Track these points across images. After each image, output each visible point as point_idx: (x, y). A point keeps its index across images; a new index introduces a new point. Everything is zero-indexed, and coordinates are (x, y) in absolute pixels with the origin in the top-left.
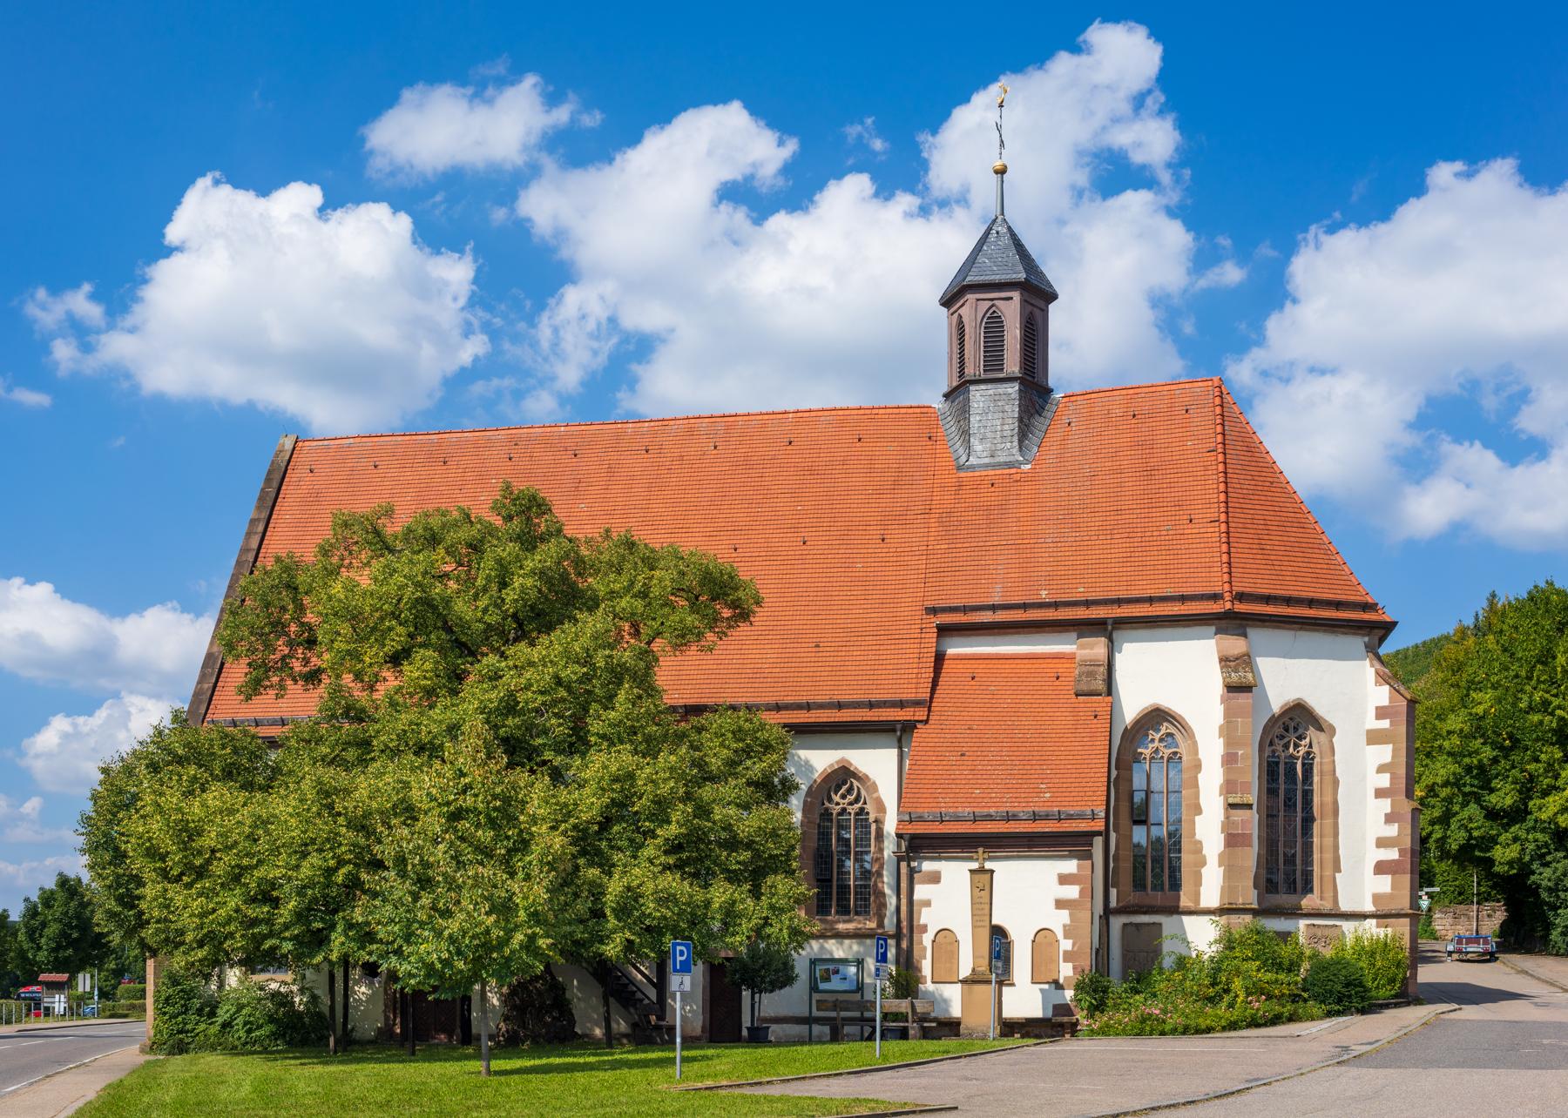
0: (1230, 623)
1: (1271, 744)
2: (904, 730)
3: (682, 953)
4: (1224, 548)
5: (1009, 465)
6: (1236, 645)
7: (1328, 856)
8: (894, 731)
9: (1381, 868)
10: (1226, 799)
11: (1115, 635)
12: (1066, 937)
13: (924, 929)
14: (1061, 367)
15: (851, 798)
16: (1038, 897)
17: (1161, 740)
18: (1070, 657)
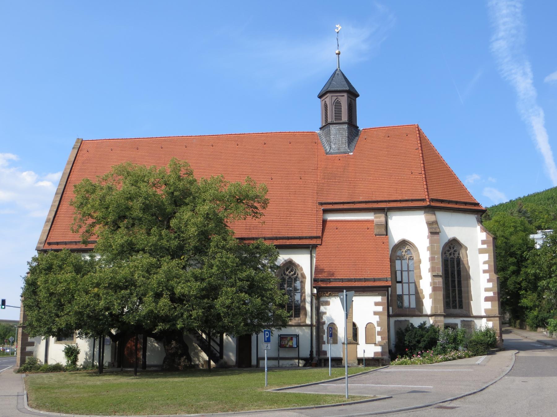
0: (430, 209)
1: (445, 253)
2: (312, 248)
3: (267, 335)
4: (425, 183)
5: (345, 153)
6: (432, 218)
9: (487, 299)
11: (388, 213)
12: (378, 326)
14: (362, 123)
16: (368, 310)
17: (406, 252)
18: (372, 221)
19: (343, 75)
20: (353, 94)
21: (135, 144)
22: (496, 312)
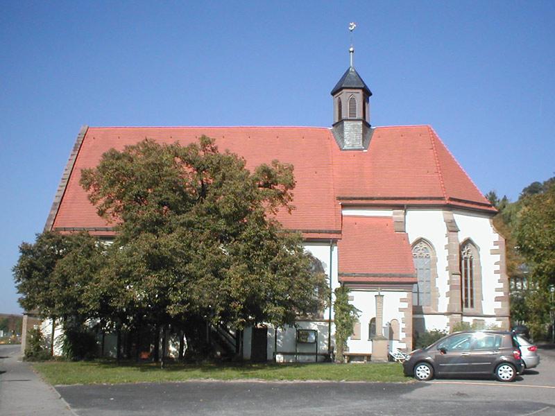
2: (333, 242)
8: (329, 242)
9: (497, 299)
18: (390, 218)
20: (367, 93)
22: (506, 311)
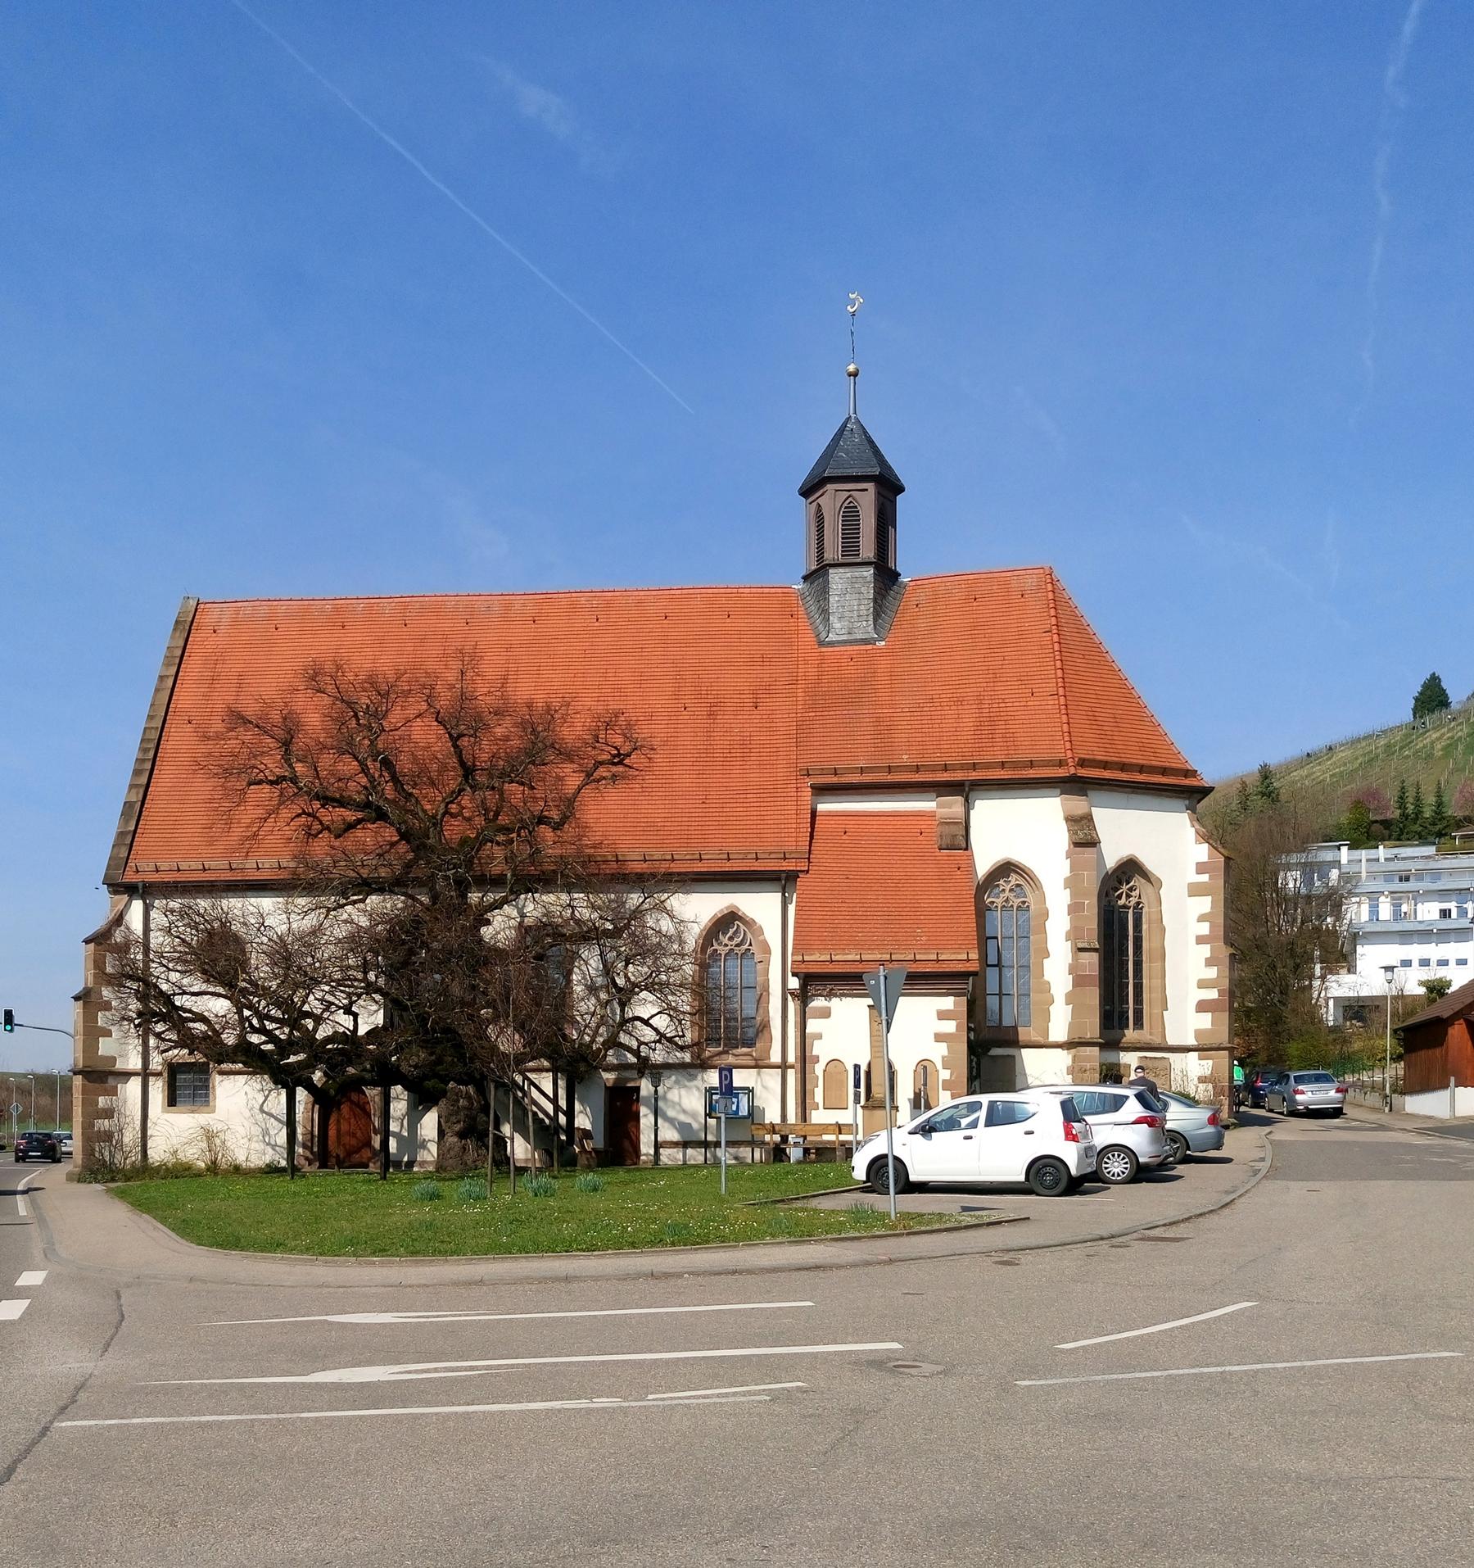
5: (865, 642)
6: (1078, 804)
7: (1156, 995)
8: (779, 879)
9: (1202, 1007)
10: (1074, 944)
13: (816, 1059)
14: (908, 563)
15: (737, 940)
17: (1011, 890)
18: (930, 815)
19: (865, 432)
20: (889, 487)
21: (339, 616)
22: (1223, 1037)
